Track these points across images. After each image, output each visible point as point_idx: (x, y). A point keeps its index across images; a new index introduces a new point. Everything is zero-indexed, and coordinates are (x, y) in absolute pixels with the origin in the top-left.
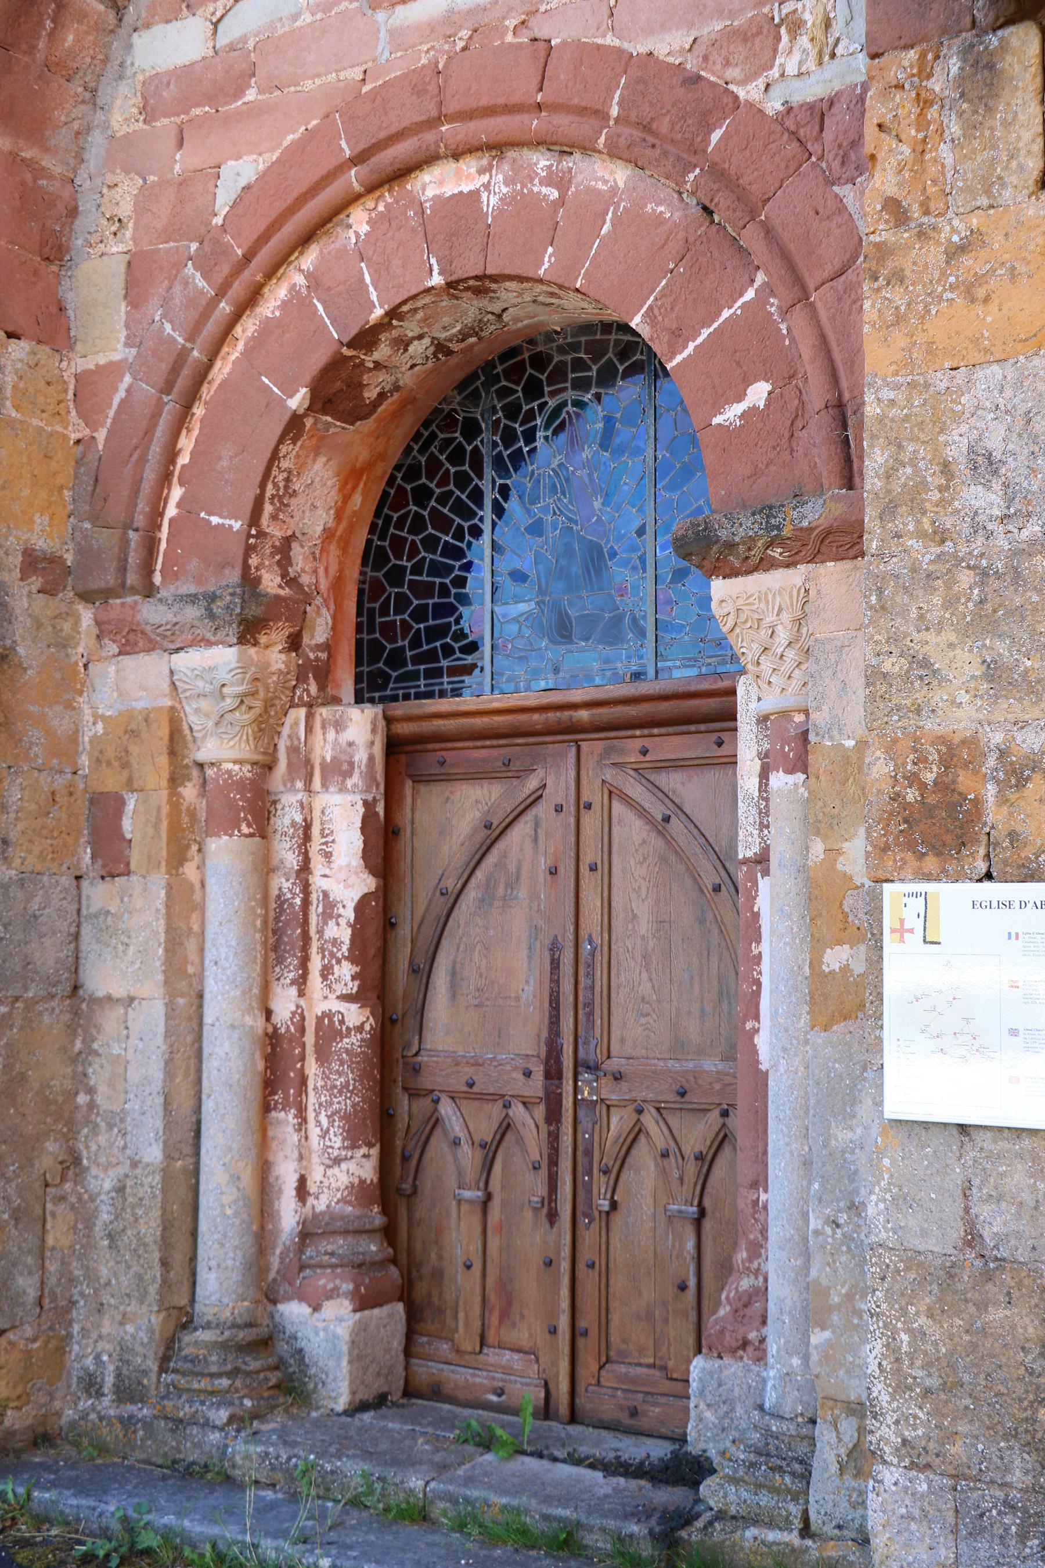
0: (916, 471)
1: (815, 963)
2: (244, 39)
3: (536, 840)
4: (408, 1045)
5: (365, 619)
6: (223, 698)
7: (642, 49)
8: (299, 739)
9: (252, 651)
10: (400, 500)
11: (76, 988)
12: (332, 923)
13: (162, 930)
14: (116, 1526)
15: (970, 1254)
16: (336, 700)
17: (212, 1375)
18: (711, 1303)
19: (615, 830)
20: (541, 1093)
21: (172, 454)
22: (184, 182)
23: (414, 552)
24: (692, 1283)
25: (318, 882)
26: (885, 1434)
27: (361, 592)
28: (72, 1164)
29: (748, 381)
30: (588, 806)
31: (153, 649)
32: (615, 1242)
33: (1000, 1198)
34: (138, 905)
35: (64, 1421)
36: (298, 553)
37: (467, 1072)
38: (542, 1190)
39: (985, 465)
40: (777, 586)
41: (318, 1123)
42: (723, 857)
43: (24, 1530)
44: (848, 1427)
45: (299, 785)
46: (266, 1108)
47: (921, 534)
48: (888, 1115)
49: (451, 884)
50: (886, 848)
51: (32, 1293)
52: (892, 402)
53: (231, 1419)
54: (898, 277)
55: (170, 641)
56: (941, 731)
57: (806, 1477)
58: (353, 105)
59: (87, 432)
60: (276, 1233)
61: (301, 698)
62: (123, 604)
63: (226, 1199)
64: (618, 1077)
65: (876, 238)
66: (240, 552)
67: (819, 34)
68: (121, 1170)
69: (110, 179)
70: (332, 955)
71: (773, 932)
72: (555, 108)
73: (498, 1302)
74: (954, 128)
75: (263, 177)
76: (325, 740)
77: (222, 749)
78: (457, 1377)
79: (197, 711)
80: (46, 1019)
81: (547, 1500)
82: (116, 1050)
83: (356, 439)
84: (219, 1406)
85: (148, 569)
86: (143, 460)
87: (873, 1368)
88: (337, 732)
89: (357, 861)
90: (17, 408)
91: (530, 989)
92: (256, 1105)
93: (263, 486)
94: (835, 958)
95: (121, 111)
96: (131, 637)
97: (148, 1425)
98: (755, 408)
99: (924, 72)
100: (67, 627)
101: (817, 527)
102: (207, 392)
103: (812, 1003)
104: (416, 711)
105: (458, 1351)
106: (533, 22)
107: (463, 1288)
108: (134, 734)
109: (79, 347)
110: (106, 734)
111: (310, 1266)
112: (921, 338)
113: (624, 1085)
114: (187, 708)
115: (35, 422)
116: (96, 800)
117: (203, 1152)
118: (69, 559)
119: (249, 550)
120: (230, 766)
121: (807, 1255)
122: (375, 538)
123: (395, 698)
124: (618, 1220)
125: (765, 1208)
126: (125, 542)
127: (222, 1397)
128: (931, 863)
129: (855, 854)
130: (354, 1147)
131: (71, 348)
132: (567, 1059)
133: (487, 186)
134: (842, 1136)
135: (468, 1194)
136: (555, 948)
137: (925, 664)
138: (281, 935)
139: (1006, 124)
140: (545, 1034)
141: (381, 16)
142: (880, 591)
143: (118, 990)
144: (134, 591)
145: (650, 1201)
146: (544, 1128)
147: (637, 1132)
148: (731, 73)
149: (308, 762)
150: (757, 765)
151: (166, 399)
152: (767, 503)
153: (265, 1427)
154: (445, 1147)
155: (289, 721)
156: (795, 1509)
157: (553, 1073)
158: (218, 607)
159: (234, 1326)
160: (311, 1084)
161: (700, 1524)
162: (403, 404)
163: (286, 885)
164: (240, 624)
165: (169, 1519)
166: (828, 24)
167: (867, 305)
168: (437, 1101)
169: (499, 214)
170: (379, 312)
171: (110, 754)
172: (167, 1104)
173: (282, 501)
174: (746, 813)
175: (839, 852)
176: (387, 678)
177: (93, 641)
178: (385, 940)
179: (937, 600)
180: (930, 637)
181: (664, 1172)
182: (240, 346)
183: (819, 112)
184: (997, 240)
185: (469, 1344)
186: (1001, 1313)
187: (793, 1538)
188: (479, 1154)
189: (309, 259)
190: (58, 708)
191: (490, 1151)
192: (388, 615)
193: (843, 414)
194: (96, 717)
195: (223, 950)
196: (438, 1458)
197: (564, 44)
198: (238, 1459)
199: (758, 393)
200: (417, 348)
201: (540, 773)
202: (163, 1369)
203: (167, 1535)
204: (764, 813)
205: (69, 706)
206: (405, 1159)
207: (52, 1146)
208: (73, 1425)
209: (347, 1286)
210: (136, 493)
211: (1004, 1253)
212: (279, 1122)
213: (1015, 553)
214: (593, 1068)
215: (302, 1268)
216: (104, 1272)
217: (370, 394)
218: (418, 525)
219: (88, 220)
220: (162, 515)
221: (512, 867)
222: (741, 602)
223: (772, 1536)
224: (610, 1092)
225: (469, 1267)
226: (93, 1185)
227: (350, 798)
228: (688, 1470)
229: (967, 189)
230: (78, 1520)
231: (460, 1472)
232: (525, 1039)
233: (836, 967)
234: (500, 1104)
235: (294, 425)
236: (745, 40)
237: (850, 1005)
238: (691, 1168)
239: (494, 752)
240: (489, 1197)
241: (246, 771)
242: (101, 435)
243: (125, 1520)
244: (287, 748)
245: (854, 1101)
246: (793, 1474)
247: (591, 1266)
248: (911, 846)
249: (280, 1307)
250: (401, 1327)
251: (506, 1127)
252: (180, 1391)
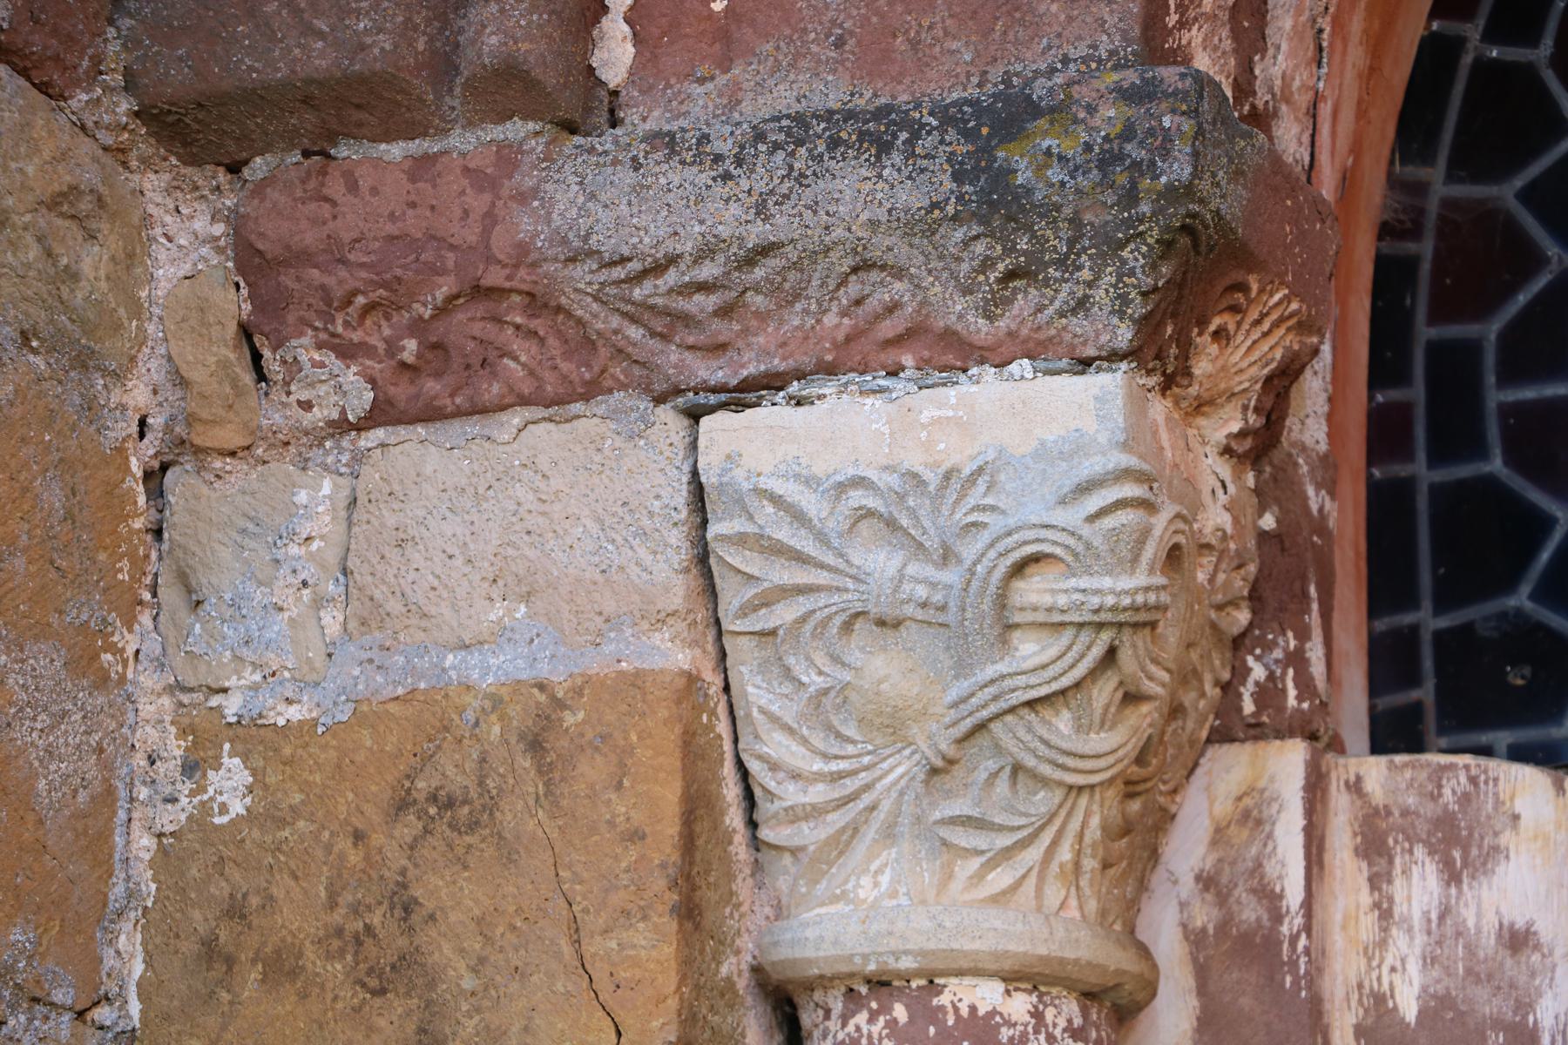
5: (1417, 393)
8: (1271, 898)
31: (591, 391)
55: (696, 348)
61: (1269, 694)
62: (422, 166)
76: (1384, 912)
88: (1452, 877)
96: (467, 325)
100: (93, 261)
108: (454, 814)
110: (266, 815)
114: (755, 691)
120: (987, 995)
122: (1473, 32)
144: (507, 89)
164: (1167, 246)
171: (297, 915)
190: (47, 661)
205: (88, 661)
244: (1195, 939)
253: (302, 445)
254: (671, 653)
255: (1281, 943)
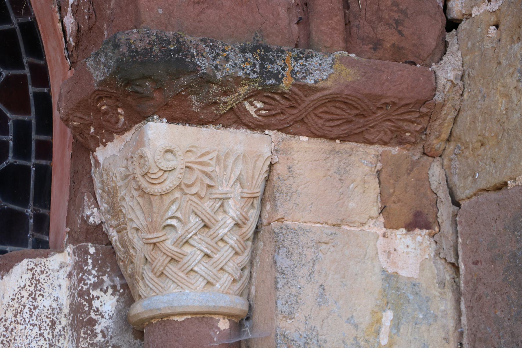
40: (240, 149)
101: (323, 89)
152: (267, 41)
192: (14, 30)
222: (192, 158)
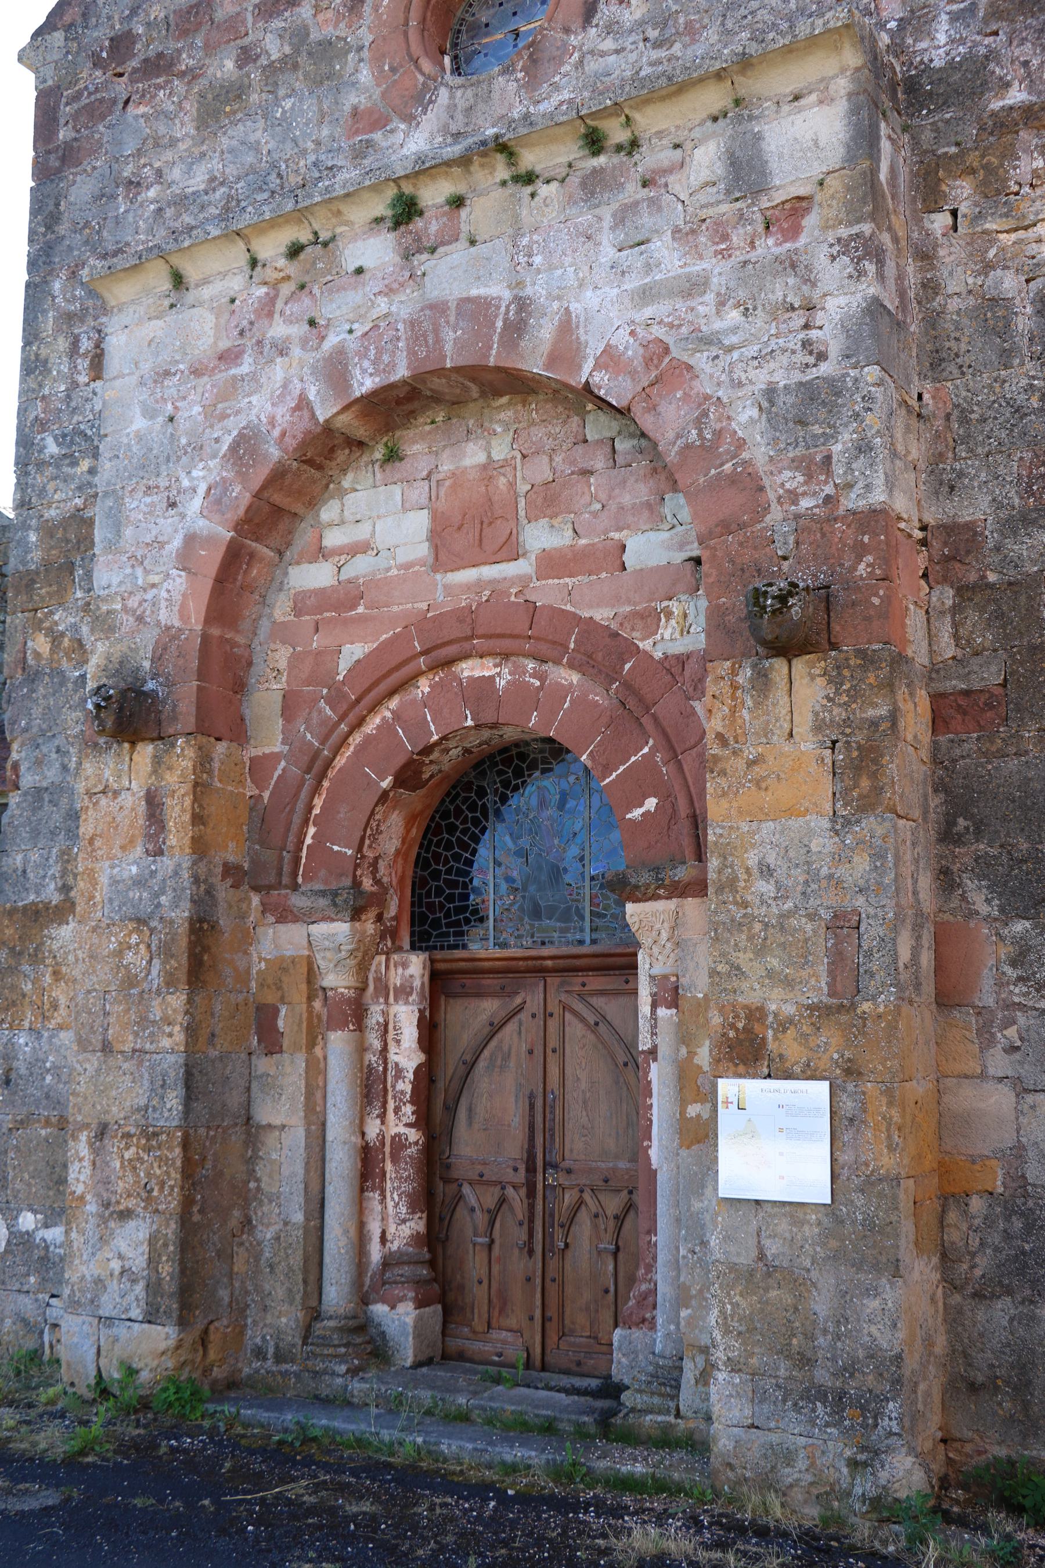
0: (733, 871)
1: (683, 1113)
2: (357, 578)
3: (520, 1033)
4: (443, 1152)
6: (340, 951)
7: (587, 615)
9: (357, 924)
10: (438, 831)
11: (249, 1119)
12: (400, 1081)
13: (303, 1086)
14: (292, 1426)
15: (761, 1264)
16: (399, 949)
17: (335, 1346)
18: (625, 1296)
19: (567, 1029)
20: (523, 1181)
21: (310, 808)
22: (319, 653)
23: (446, 861)
24: (612, 1289)
25: (393, 1057)
26: (719, 1355)
27: (414, 883)
28: (247, 1223)
29: (645, 797)
30: (551, 1015)
32: (568, 1267)
33: (775, 1236)
34: (291, 1070)
35: (243, 1375)
36: (382, 865)
37: (479, 1168)
38: (525, 1237)
39: (766, 871)
40: (661, 909)
41: (393, 1199)
42: (629, 1045)
43: (239, 1430)
44: (700, 1360)
45: (382, 1000)
46: (362, 1190)
47: (736, 903)
48: (722, 1194)
49: (468, 1057)
50: (719, 1061)
51: (227, 1299)
52: (721, 835)
53: (348, 1371)
54: (723, 773)
55: (309, 917)
56: (745, 1002)
57: (678, 1387)
58: (422, 623)
59: (257, 792)
60: (369, 1263)
63: (341, 1244)
64: (569, 1171)
65: (712, 752)
66: (352, 868)
67: (681, 621)
68: (277, 1227)
69: (273, 646)
70: (401, 1100)
71: (659, 1094)
72: (538, 639)
73: (501, 1302)
74: (749, 703)
75: (367, 656)
77: (337, 980)
78: (475, 1347)
79: (324, 958)
80: (233, 1138)
81: (537, 1407)
82: (274, 1156)
83: (414, 799)
84: (340, 1363)
85: (295, 875)
86: (292, 811)
87: (713, 1323)
89: (415, 1045)
90: (220, 781)
91: (517, 1120)
92: (357, 1189)
93: (365, 830)
94: (693, 1110)
95: (281, 609)
97: (297, 1375)
98: (648, 812)
99: (734, 673)
100: (244, 906)
102: (331, 774)
103: (681, 1133)
104: (449, 957)
105: (474, 1332)
106: (526, 591)
107: (479, 1294)
108: (285, 970)
109: (252, 741)
111: (390, 1283)
112: (735, 804)
113: (573, 1176)
115: (230, 788)
116: (261, 1008)
117: (326, 1216)
118: (246, 866)
119: (357, 866)
121: (678, 1270)
123: (435, 948)
124: (569, 1254)
125: (655, 1244)
126: (281, 859)
127: (342, 1359)
128: (741, 1069)
129: (704, 1056)
130: (413, 1213)
131: (248, 742)
132: (539, 1160)
133: (499, 674)
134: (697, 1205)
135: (480, 1240)
136: (531, 1097)
137: (738, 968)
138: (371, 1088)
139: (774, 705)
140: (526, 1146)
141: (438, 576)
142: (716, 930)
143: (277, 1121)
144: (286, 887)
145: (588, 1242)
146: (526, 1201)
147: (581, 1202)
148: (635, 634)
149: (387, 988)
150: (650, 999)
151: (308, 777)
153: (366, 1376)
154: (466, 1212)
155: (375, 963)
156: (672, 1404)
157: (531, 1169)
158: (339, 900)
159: (346, 1318)
160: (388, 1176)
161: (621, 1415)
162: (443, 779)
163: (374, 1059)
165: (324, 1422)
166: (685, 616)
167: (708, 785)
168: (461, 1186)
169: (506, 690)
170: (435, 738)
171: (270, 981)
172: (306, 1188)
173: (374, 838)
174: (644, 1026)
175: (695, 1054)
176: (430, 935)
177: (259, 914)
178: (429, 1090)
179: (744, 937)
180: (741, 955)
181: (596, 1227)
182: (352, 749)
183: (682, 660)
184: (771, 761)
185: (480, 1327)
186: (775, 1293)
187: (671, 1419)
188: (486, 1216)
189: (394, 703)
190: (240, 954)
191: (493, 1216)
193: (697, 822)
194: (261, 959)
195: (339, 1098)
196: (471, 1388)
197: (544, 606)
198: (356, 1393)
199: (651, 803)
200: (453, 753)
201: (523, 994)
202: (305, 1343)
203: (327, 1429)
204: (654, 1027)
205: (246, 953)
206: (441, 1219)
207: (236, 1213)
208: (249, 1377)
209: (411, 1294)
210: (288, 830)
211: (777, 1263)
212: (369, 1199)
213: (782, 916)
214: (555, 1166)
215: (384, 1284)
216: (267, 1287)
217: (426, 776)
218: (449, 846)
219: (259, 667)
220: (303, 842)
221: (505, 1048)
223: (660, 1418)
224: (564, 1180)
225: (480, 1282)
226: (259, 1236)
227: (411, 1008)
228: (612, 1390)
229: (756, 734)
230: (269, 1425)
231: (486, 1395)
232: (514, 1149)
233: (694, 1115)
234: (499, 1187)
235: (384, 795)
236: (642, 618)
237: (700, 1135)
238: (611, 1223)
239: (496, 982)
240: (492, 1241)
241: (352, 993)
242: (266, 795)
243: (298, 1423)
245: (703, 1187)
246: (671, 1386)
247: (554, 1280)
248: (731, 1060)
249: (371, 1307)
250: (440, 1318)
251: (503, 1201)
252: (315, 1355)
253: (269, 925)
254: (306, 953)
255: (641, 806)
